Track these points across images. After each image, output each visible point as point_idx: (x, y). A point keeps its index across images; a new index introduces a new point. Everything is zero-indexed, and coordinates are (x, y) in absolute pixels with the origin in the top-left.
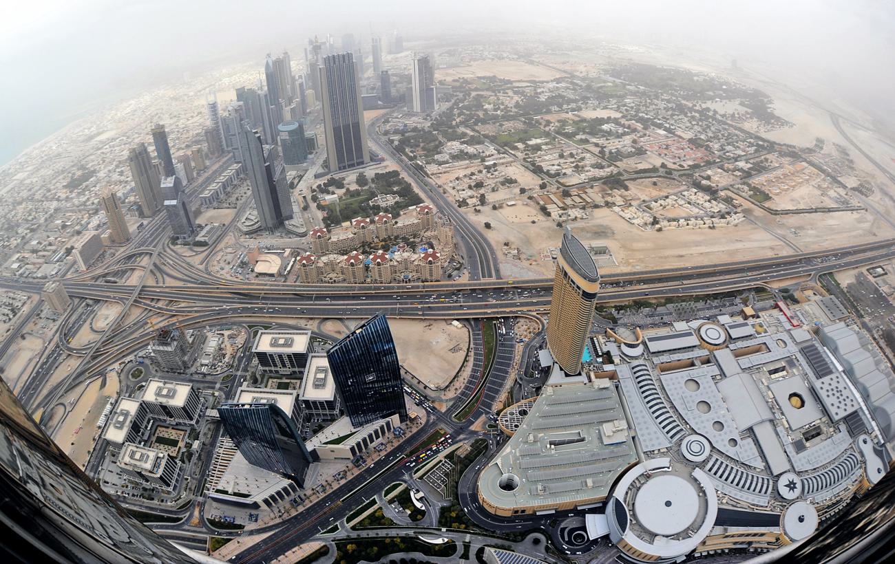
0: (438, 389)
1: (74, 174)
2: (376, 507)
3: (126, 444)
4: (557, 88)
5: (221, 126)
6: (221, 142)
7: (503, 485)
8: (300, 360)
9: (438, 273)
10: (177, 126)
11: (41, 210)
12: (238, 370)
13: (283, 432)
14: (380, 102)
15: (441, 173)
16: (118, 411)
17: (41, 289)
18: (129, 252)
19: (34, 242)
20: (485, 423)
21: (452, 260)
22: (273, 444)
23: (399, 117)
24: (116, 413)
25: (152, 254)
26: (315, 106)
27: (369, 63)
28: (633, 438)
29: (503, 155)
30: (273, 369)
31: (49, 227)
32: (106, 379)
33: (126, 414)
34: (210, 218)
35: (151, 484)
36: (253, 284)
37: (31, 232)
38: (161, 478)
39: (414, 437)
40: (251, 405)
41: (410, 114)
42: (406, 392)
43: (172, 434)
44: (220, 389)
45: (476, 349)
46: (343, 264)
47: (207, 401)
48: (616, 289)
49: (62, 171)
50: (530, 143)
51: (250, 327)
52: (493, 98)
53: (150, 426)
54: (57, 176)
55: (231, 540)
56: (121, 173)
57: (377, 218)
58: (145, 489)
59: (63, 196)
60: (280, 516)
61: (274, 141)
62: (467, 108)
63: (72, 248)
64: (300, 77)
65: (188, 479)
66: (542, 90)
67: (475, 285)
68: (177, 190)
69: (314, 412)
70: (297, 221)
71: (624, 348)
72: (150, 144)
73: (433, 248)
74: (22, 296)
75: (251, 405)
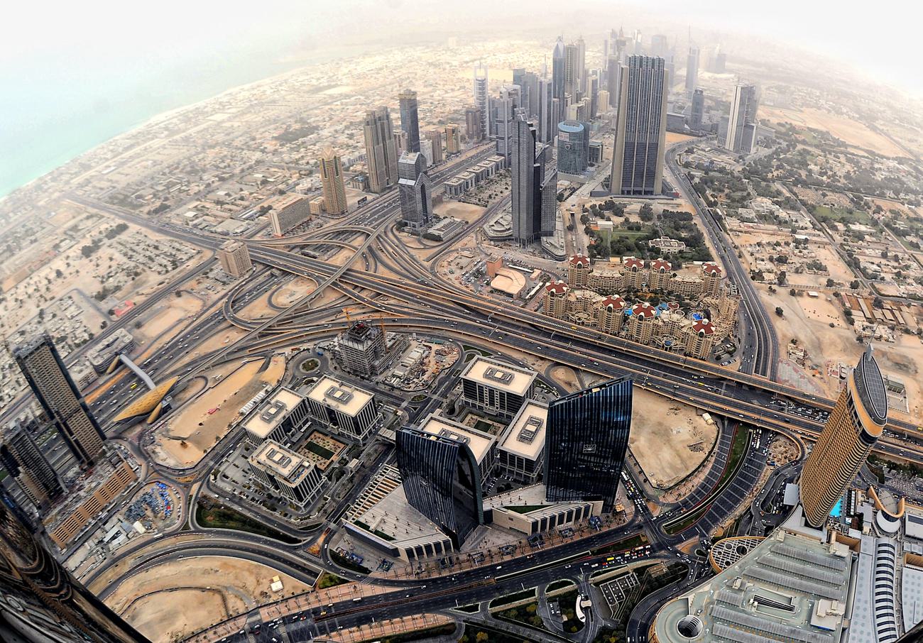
0: (660, 487)
1: (289, 126)
2: (531, 599)
3: (269, 440)
4: (898, 169)
5: (487, 107)
6: (483, 126)
7: (684, 626)
8: (514, 403)
9: (706, 349)
10: (432, 96)
11: (239, 159)
12: (435, 393)
13: (463, 479)
14: (686, 126)
15: (741, 232)
16: (273, 402)
17: (217, 245)
18: (340, 227)
19: (221, 193)
20: (694, 547)
21: (727, 340)
22: (446, 491)
23: (707, 150)
24: (269, 403)
25: (368, 235)
26: (607, 111)
27: (681, 76)
28: (844, 630)
29: (818, 233)
30: (478, 403)
31: (245, 179)
32: (269, 362)
33: (281, 407)
34: (451, 211)
35: (280, 492)
36: (484, 299)
37: (219, 181)
38: (296, 489)
39: (608, 534)
40: (438, 438)
41: (720, 150)
42: (623, 480)
43: (328, 444)
44: (406, 409)
45: (719, 455)
46: (599, 306)
47: (385, 418)
48: (897, 442)
49: (275, 120)
50: (853, 227)
51: (466, 348)
52: (821, 159)
53: (305, 428)
54: (266, 125)
55: (347, 582)
56: (351, 136)
57: (654, 264)
58: (270, 496)
59: (270, 148)
60: (418, 573)
61: (549, 139)
62: (788, 162)
63: (270, 208)
64: (595, 73)
65: (326, 499)
66: (880, 166)
67: (744, 378)
68: (419, 168)
69: (508, 467)
70: (556, 241)
71: (880, 516)
72: (393, 110)
73: (709, 318)
74: (189, 248)
75: (438, 438)
